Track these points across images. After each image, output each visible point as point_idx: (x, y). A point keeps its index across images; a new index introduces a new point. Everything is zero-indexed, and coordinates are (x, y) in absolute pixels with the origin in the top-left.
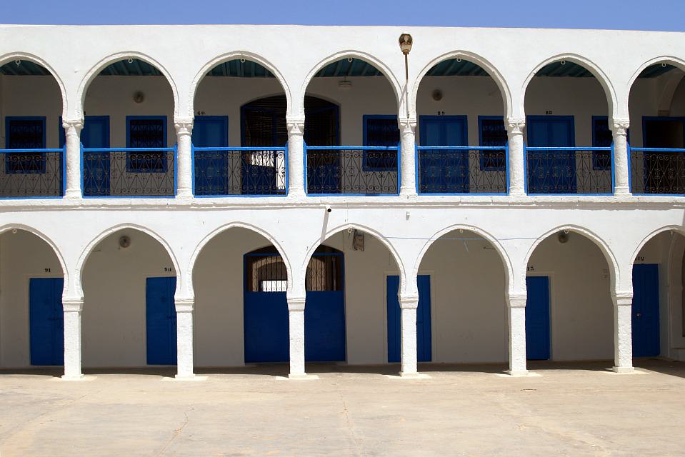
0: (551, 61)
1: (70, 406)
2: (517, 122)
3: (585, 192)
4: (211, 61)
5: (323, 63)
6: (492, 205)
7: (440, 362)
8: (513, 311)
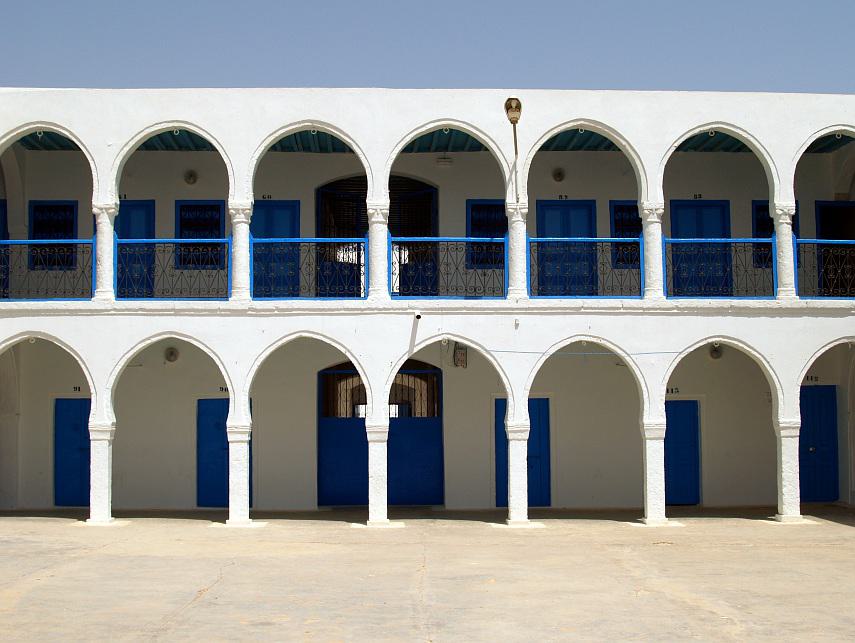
0: (696, 131)
1: (82, 558)
2: (654, 207)
3: (739, 295)
4: (275, 132)
5: (412, 135)
6: (622, 311)
7: (560, 507)
8: (649, 444)
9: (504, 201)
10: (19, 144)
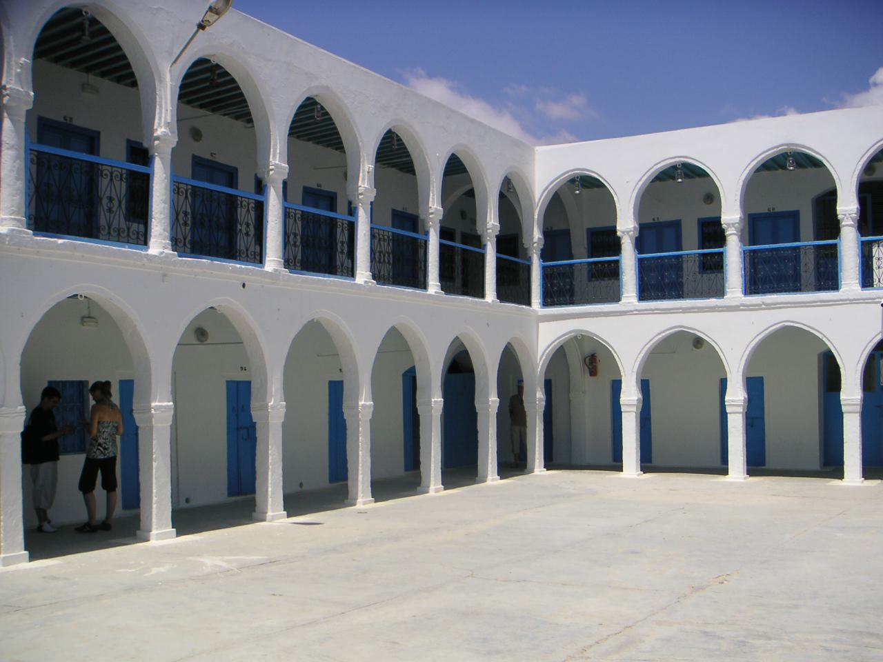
9: (616, 227)
10: (569, 183)
